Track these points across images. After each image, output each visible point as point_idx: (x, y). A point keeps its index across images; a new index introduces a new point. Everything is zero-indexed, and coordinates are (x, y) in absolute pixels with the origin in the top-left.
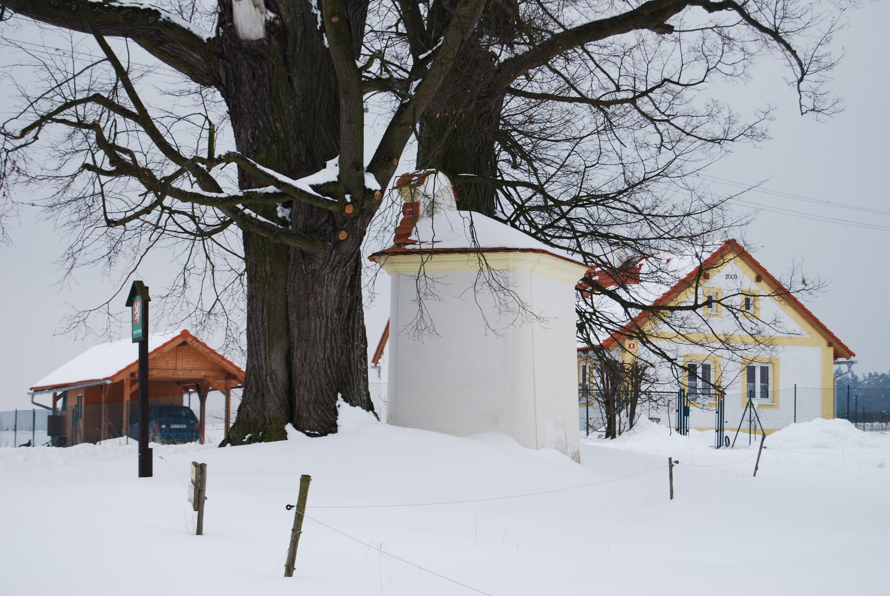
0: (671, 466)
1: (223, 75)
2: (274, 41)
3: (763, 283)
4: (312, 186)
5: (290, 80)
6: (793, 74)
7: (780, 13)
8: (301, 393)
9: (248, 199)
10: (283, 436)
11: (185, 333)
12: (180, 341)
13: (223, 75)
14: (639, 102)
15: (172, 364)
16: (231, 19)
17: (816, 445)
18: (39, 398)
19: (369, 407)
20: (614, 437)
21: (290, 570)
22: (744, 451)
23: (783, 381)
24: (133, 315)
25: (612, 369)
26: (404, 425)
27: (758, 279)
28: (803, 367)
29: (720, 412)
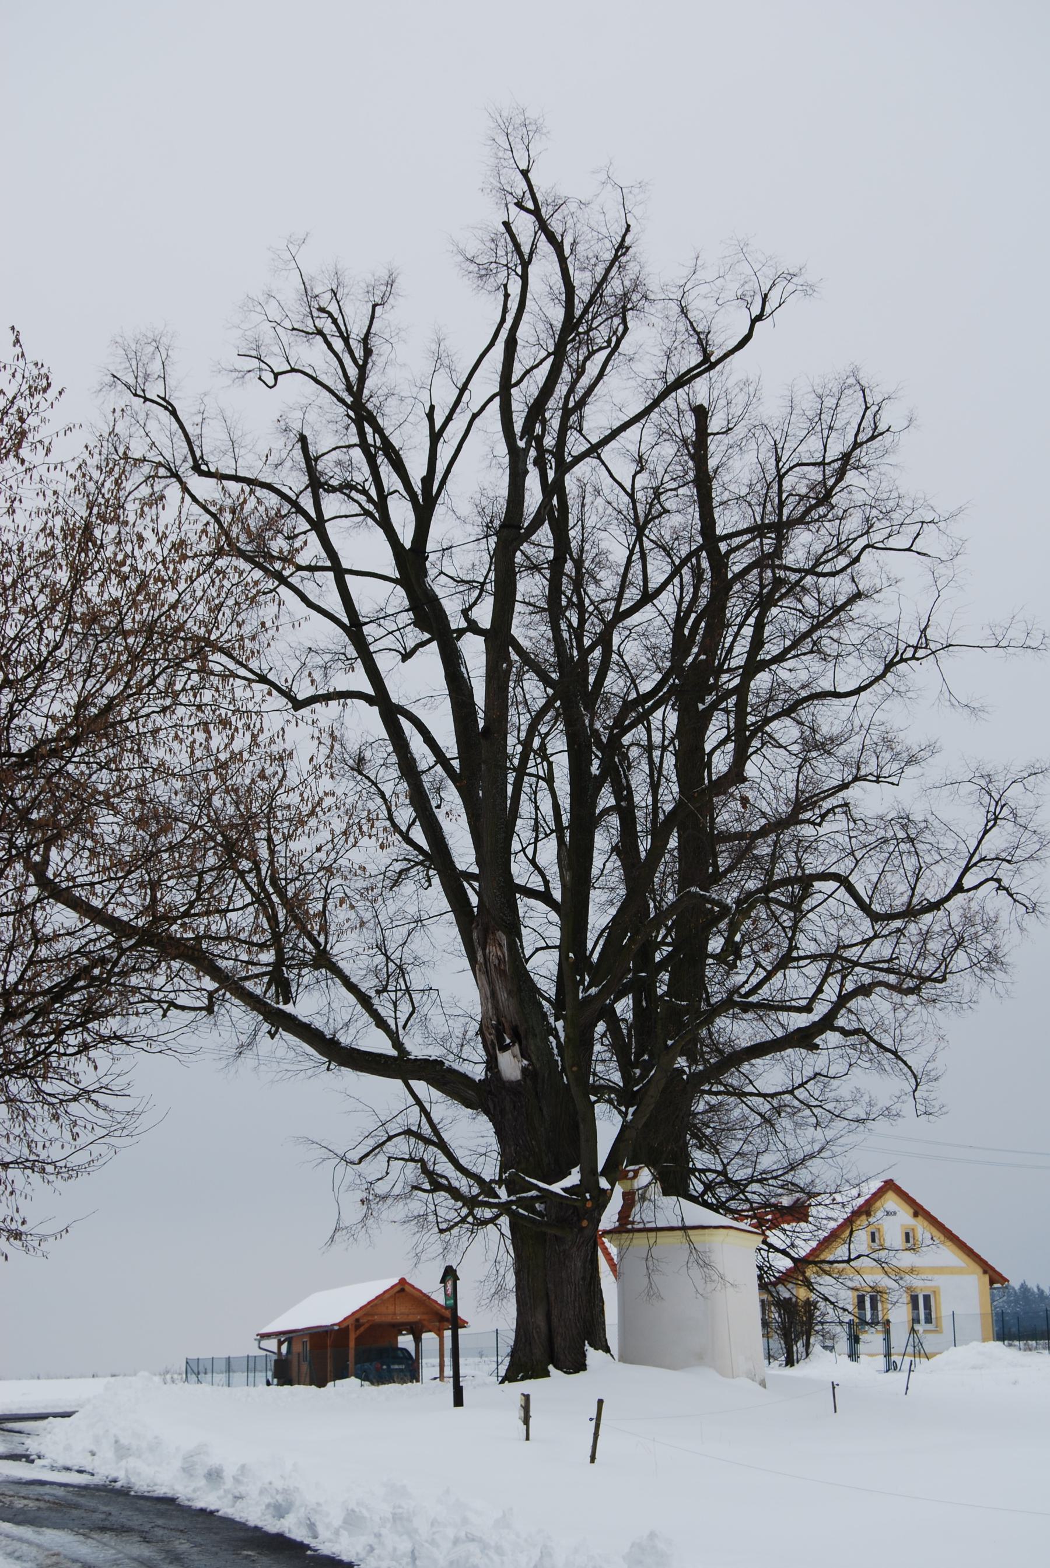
0: (834, 1388)
1: (491, 1106)
2: (528, 1081)
3: (920, 1218)
4: (563, 1189)
5: (541, 1110)
6: (908, 1085)
7: (897, 1039)
8: (559, 1341)
9: (520, 1202)
10: (547, 1374)
11: (403, 1281)
12: (398, 1288)
13: (491, 1106)
14: (796, 1092)
15: (391, 1309)
16: (497, 1066)
17: (975, 1366)
18: (265, 1344)
19: (607, 1350)
20: (792, 1365)
21: (593, 1459)
22: (898, 1378)
23: (944, 1308)
24: (445, 1290)
25: (787, 1306)
26: (632, 1363)
27: (916, 1215)
28: (963, 1295)
29: (887, 1340)
